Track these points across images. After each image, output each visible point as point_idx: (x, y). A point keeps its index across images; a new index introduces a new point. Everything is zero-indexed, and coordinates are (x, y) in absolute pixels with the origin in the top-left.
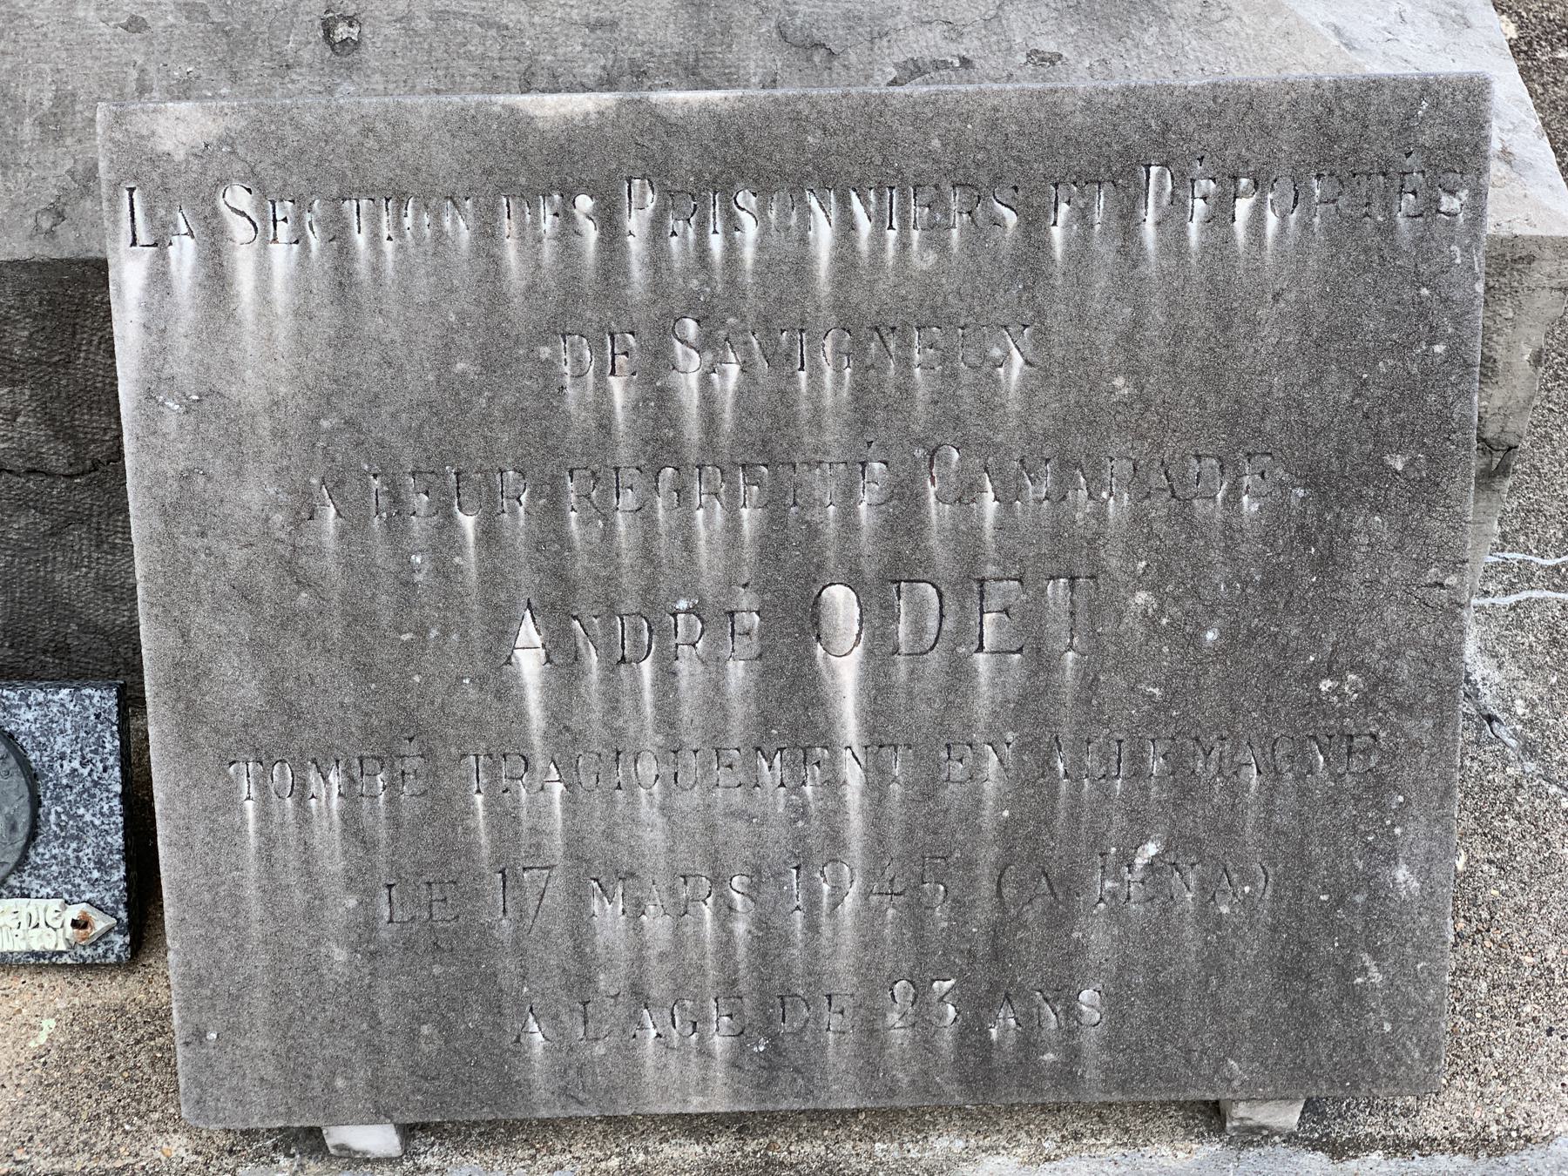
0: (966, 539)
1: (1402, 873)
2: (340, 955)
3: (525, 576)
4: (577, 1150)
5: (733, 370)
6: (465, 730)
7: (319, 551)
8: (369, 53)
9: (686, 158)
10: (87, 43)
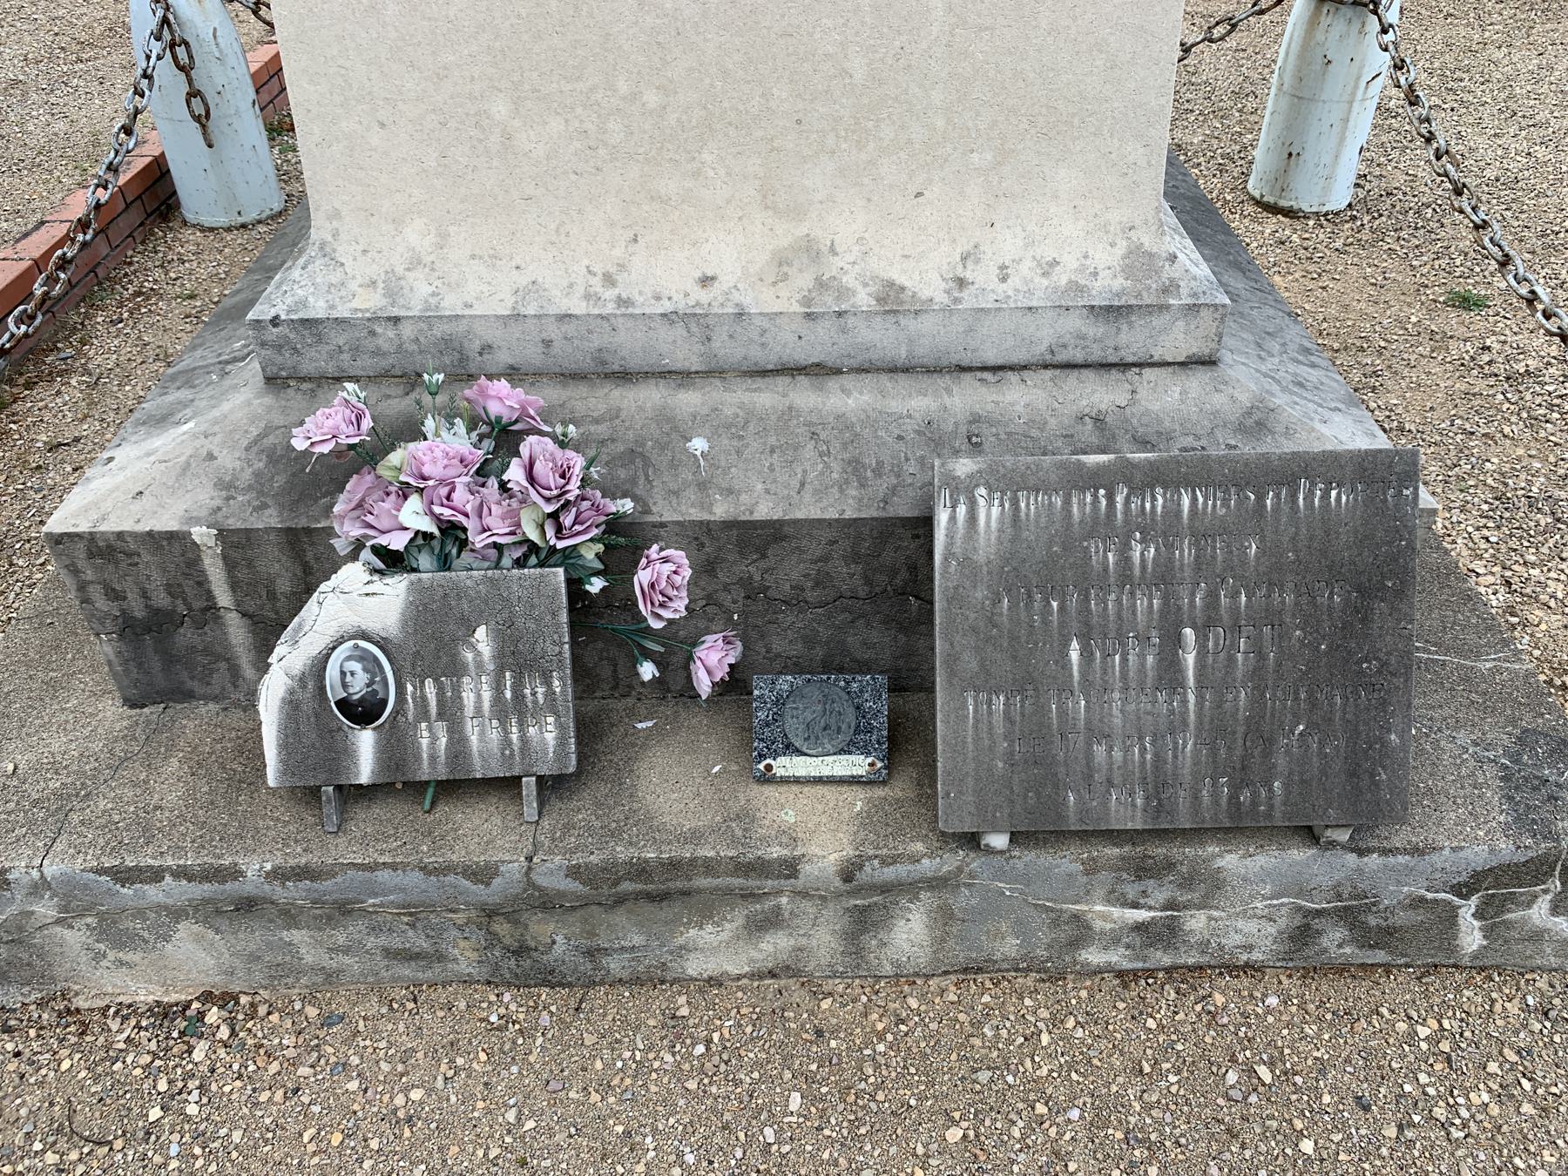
0: (1234, 610)
1: (1393, 737)
2: (1000, 765)
3: (1075, 624)
4: (1072, 850)
5: (1152, 550)
6: (1050, 680)
7: (1001, 614)
8: (986, 446)
9: (1138, 476)
10: (884, 444)
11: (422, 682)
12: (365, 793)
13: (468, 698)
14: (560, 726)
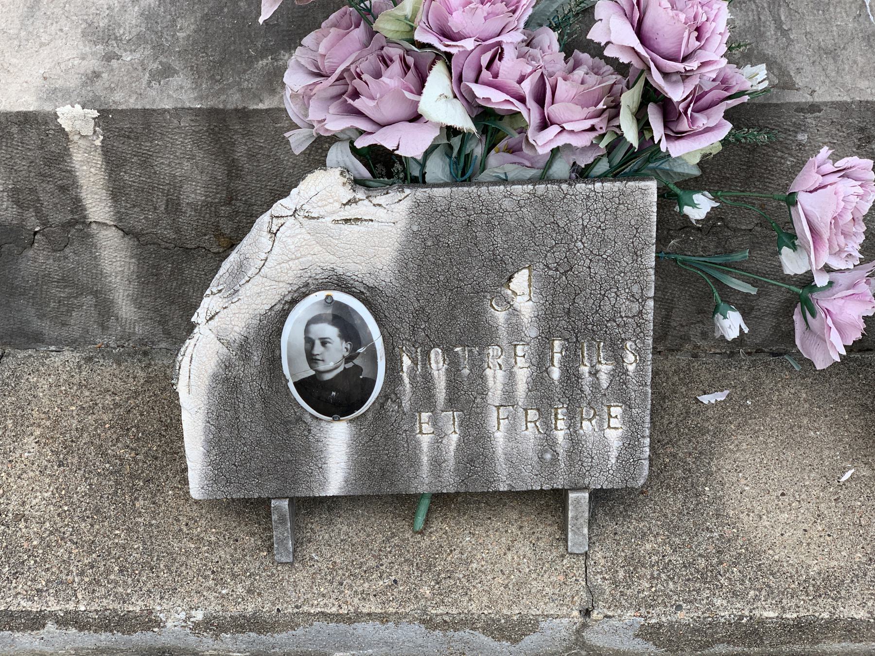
11: (426, 355)
12: (331, 504)
13: (495, 378)
14: (631, 421)
